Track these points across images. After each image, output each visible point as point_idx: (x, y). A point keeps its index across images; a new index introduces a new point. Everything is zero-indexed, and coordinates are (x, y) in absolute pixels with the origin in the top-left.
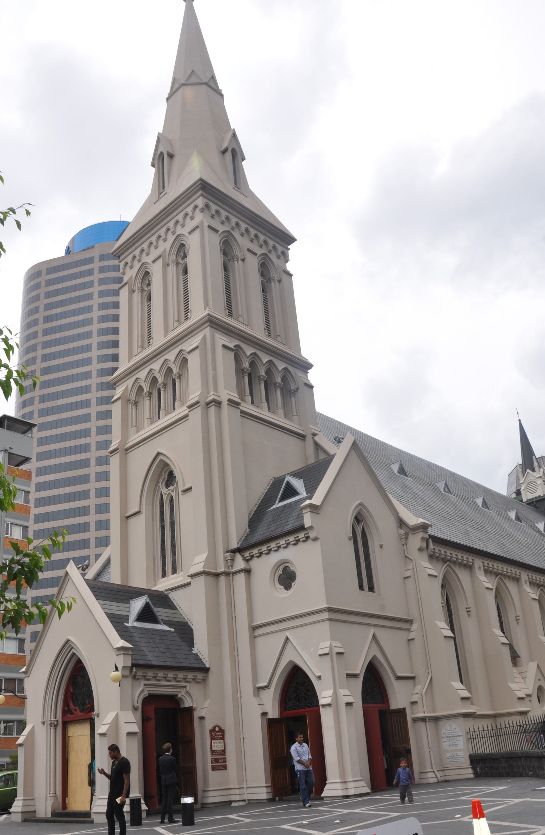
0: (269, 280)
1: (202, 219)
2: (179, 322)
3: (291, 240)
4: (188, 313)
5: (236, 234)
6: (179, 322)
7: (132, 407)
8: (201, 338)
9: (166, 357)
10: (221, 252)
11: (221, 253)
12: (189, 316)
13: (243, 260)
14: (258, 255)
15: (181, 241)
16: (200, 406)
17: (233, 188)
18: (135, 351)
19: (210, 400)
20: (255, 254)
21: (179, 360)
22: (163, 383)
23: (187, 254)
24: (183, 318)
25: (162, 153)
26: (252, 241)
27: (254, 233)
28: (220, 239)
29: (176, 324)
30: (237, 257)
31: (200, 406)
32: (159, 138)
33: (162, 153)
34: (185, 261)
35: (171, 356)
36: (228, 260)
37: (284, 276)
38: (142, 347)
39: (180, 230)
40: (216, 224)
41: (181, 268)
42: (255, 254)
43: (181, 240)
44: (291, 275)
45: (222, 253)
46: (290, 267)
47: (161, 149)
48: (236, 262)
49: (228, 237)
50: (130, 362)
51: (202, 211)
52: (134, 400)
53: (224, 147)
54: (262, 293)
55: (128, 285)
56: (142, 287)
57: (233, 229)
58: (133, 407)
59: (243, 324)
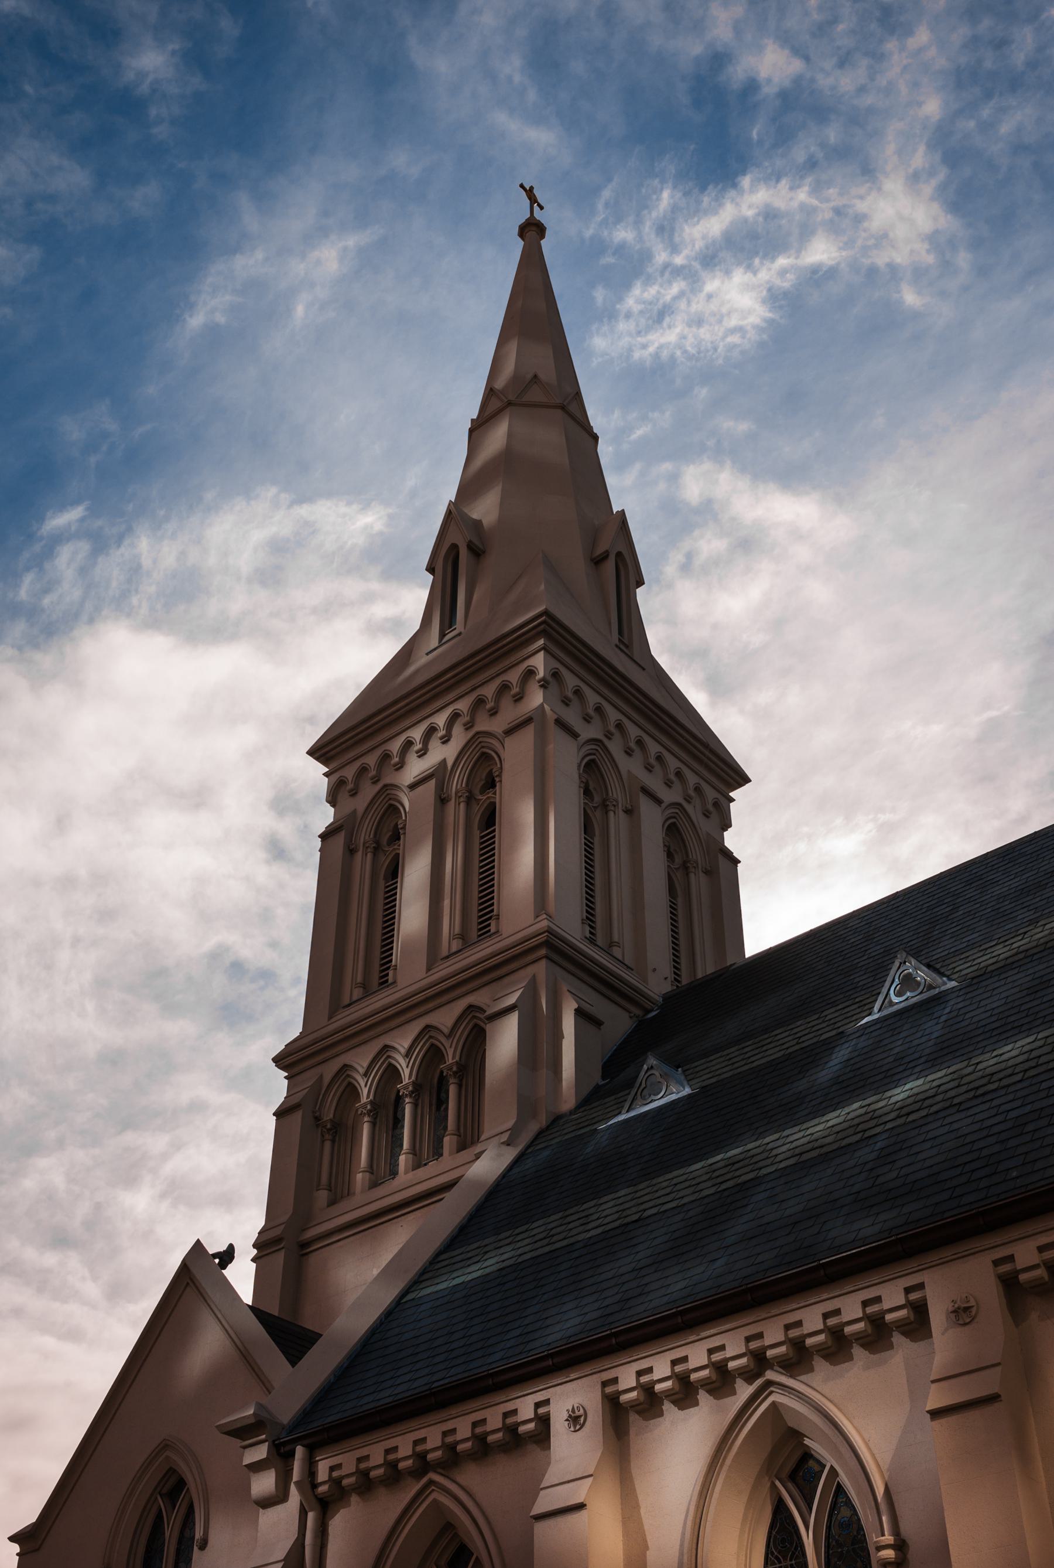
0: (685, 867)
1: (542, 703)
2: (463, 939)
3: (741, 779)
4: (490, 918)
5: (615, 747)
6: (367, 991)
7: (323, 1136)
8: (310, 1084)
9: (386, 1040)
10: (580, 787)
11: (580, 791)
12: (390, 978)
13: (628, 812)
14: (664, 805)
15: (483, 747)
16: (283, 1248)
17: (617, 646)
18: (350, 991)
19: (317, 1235)
20: (658, 801)
21: (336, 1091)
22: (371, 1102)
23: (497, 779)
24: (474, 934)
25: (454, 547)
26: (649, 768)
27: (657, 751)
28: (582, 754)
29: (357, 993)
30: (614, 803)
31: (283, 1248)
32: (450, 511)
33: (454, 547)
34: (396, 847)
35: (445, 1018)
36: (594, 807)
37: (722, 861)
38: (365, 986)
39: (483, 724)
40: (572, 717)
41: (478, 811)
42: (658, 801)
43: (483, 744)
44: (736, 862)
45: (582, 791)
46: (731, 840)
47: (451, 539)
48: (611, 814)
49: (598, 754)
50: (333, 1020)
51: (544, 684)
52: (330, 1120)
53: (599, 551)
54: (669, 898)
55: (343, 832)
56: (470, 792)
57: (609, 735)
58: (327, 1136)
59: (621, 964)
